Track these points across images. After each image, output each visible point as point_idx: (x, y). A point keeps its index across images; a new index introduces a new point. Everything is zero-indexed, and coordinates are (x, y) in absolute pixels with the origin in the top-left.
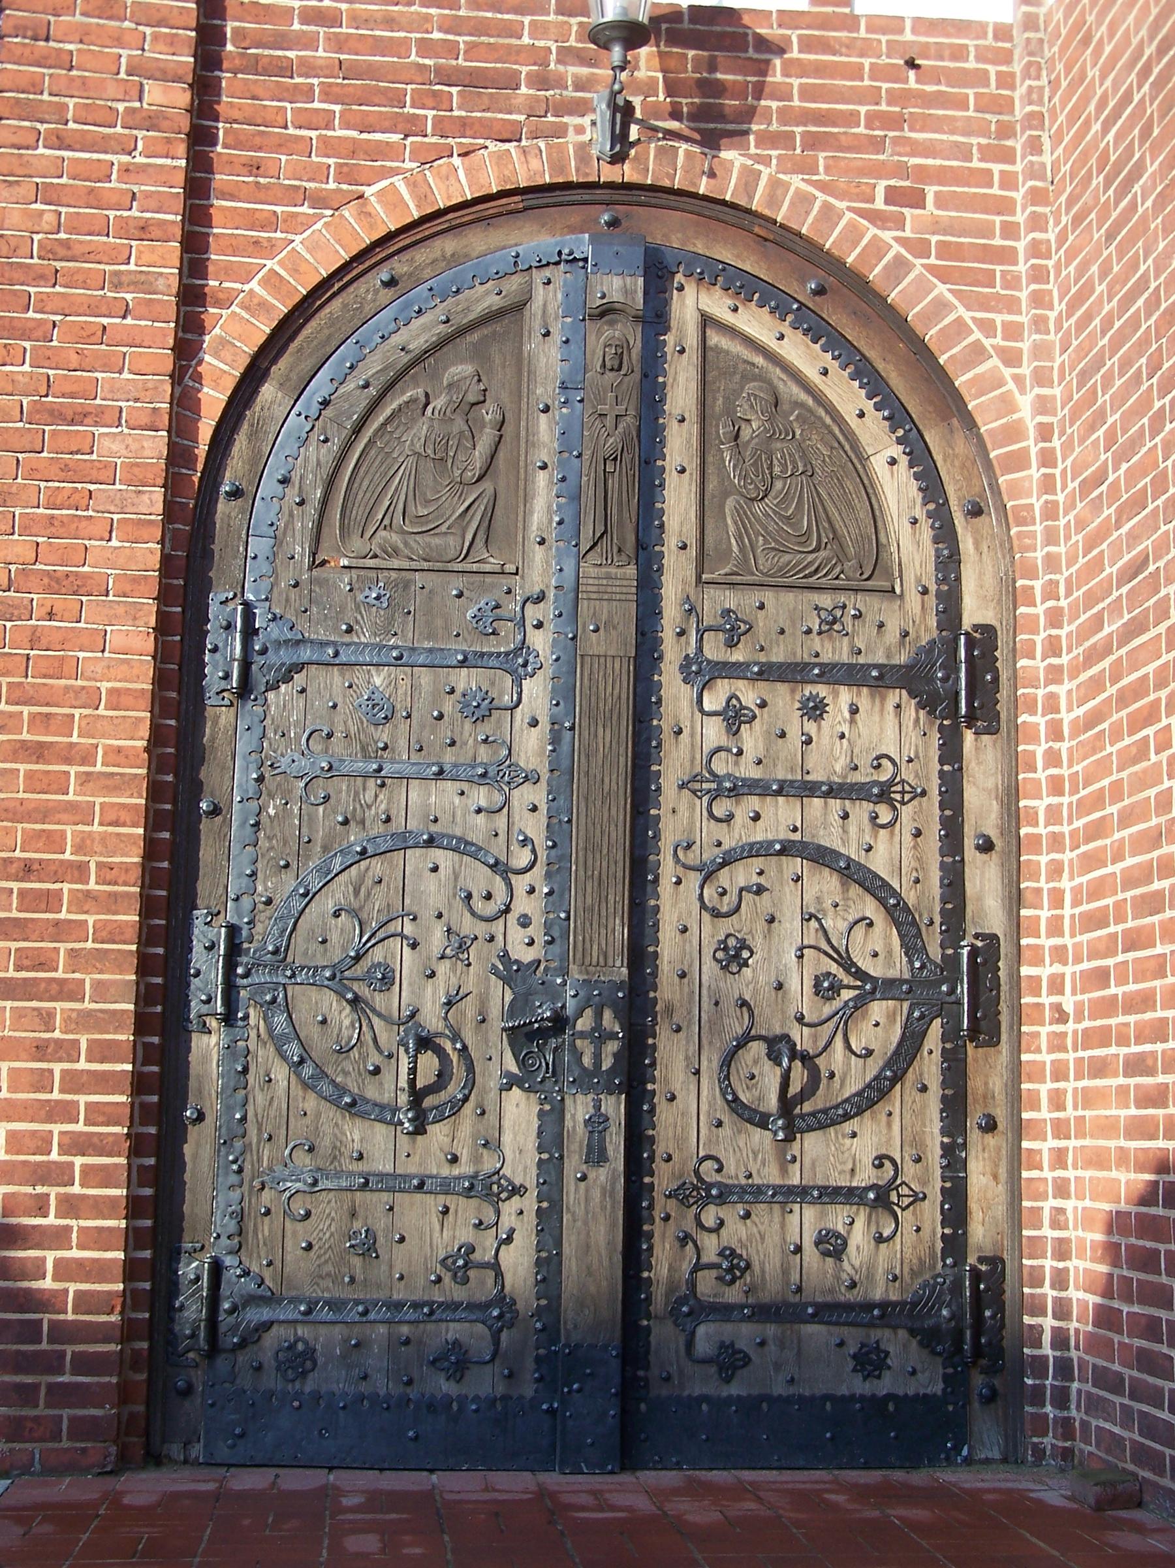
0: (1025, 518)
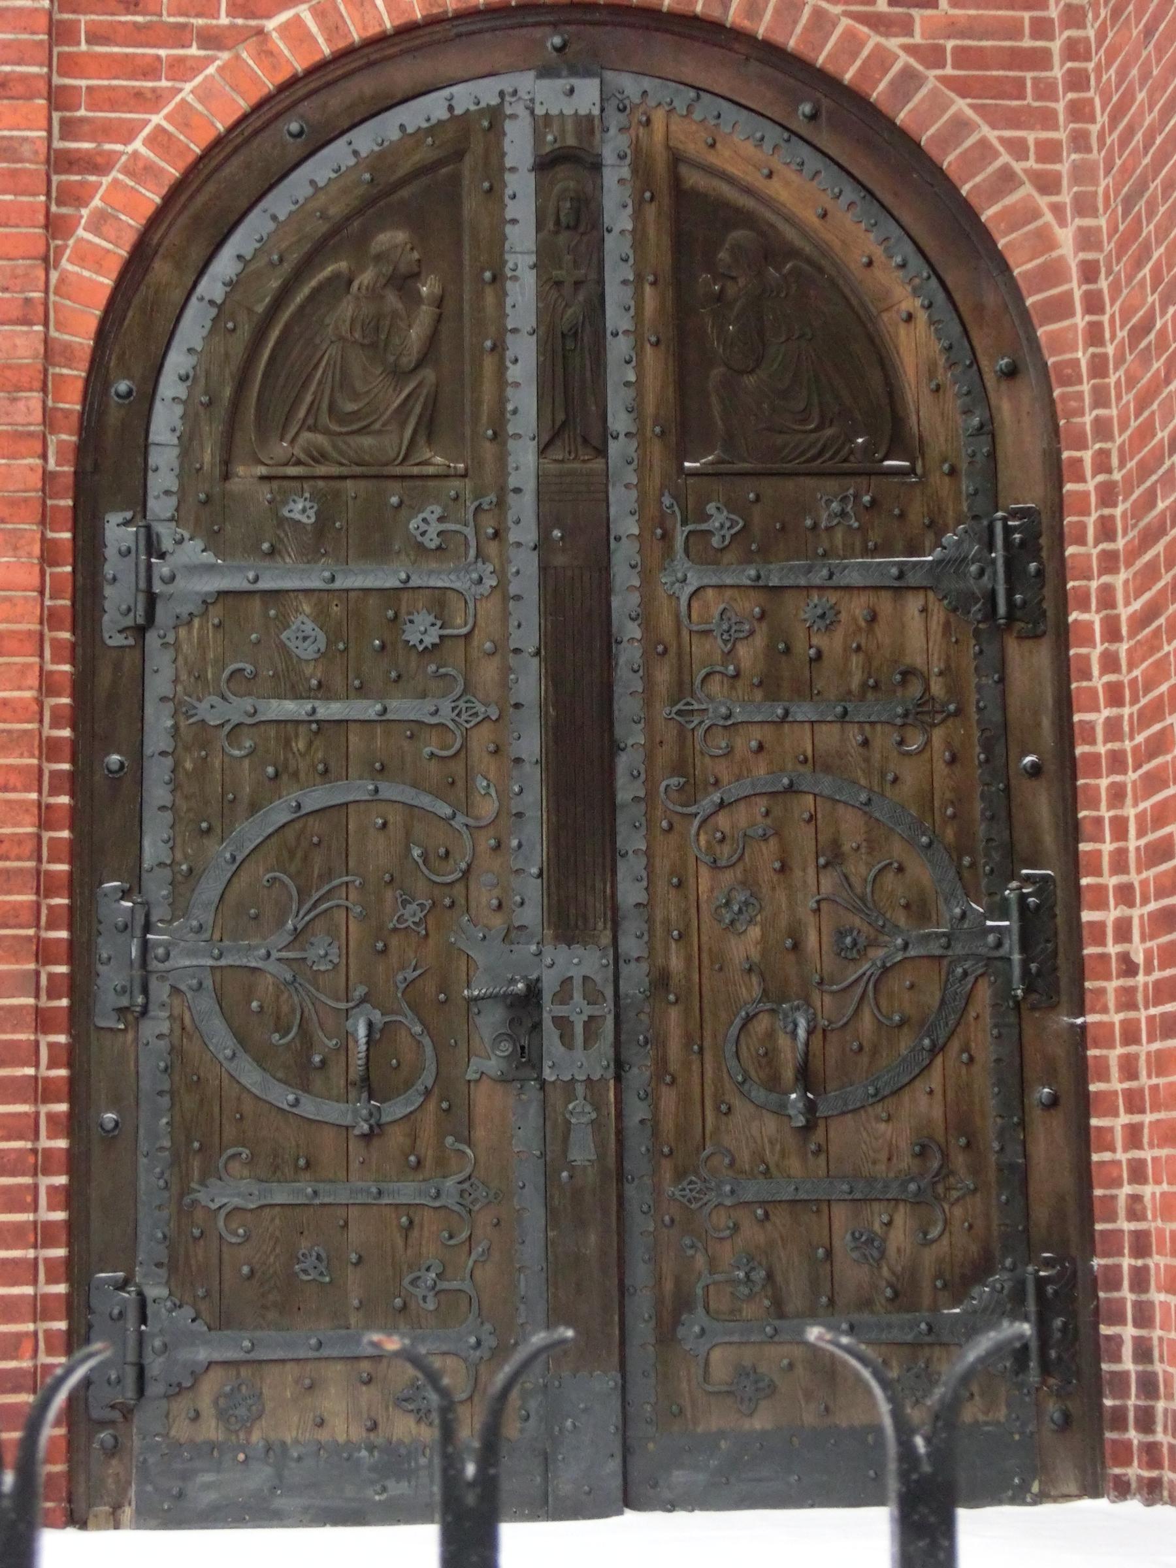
0: (1069, 377)
